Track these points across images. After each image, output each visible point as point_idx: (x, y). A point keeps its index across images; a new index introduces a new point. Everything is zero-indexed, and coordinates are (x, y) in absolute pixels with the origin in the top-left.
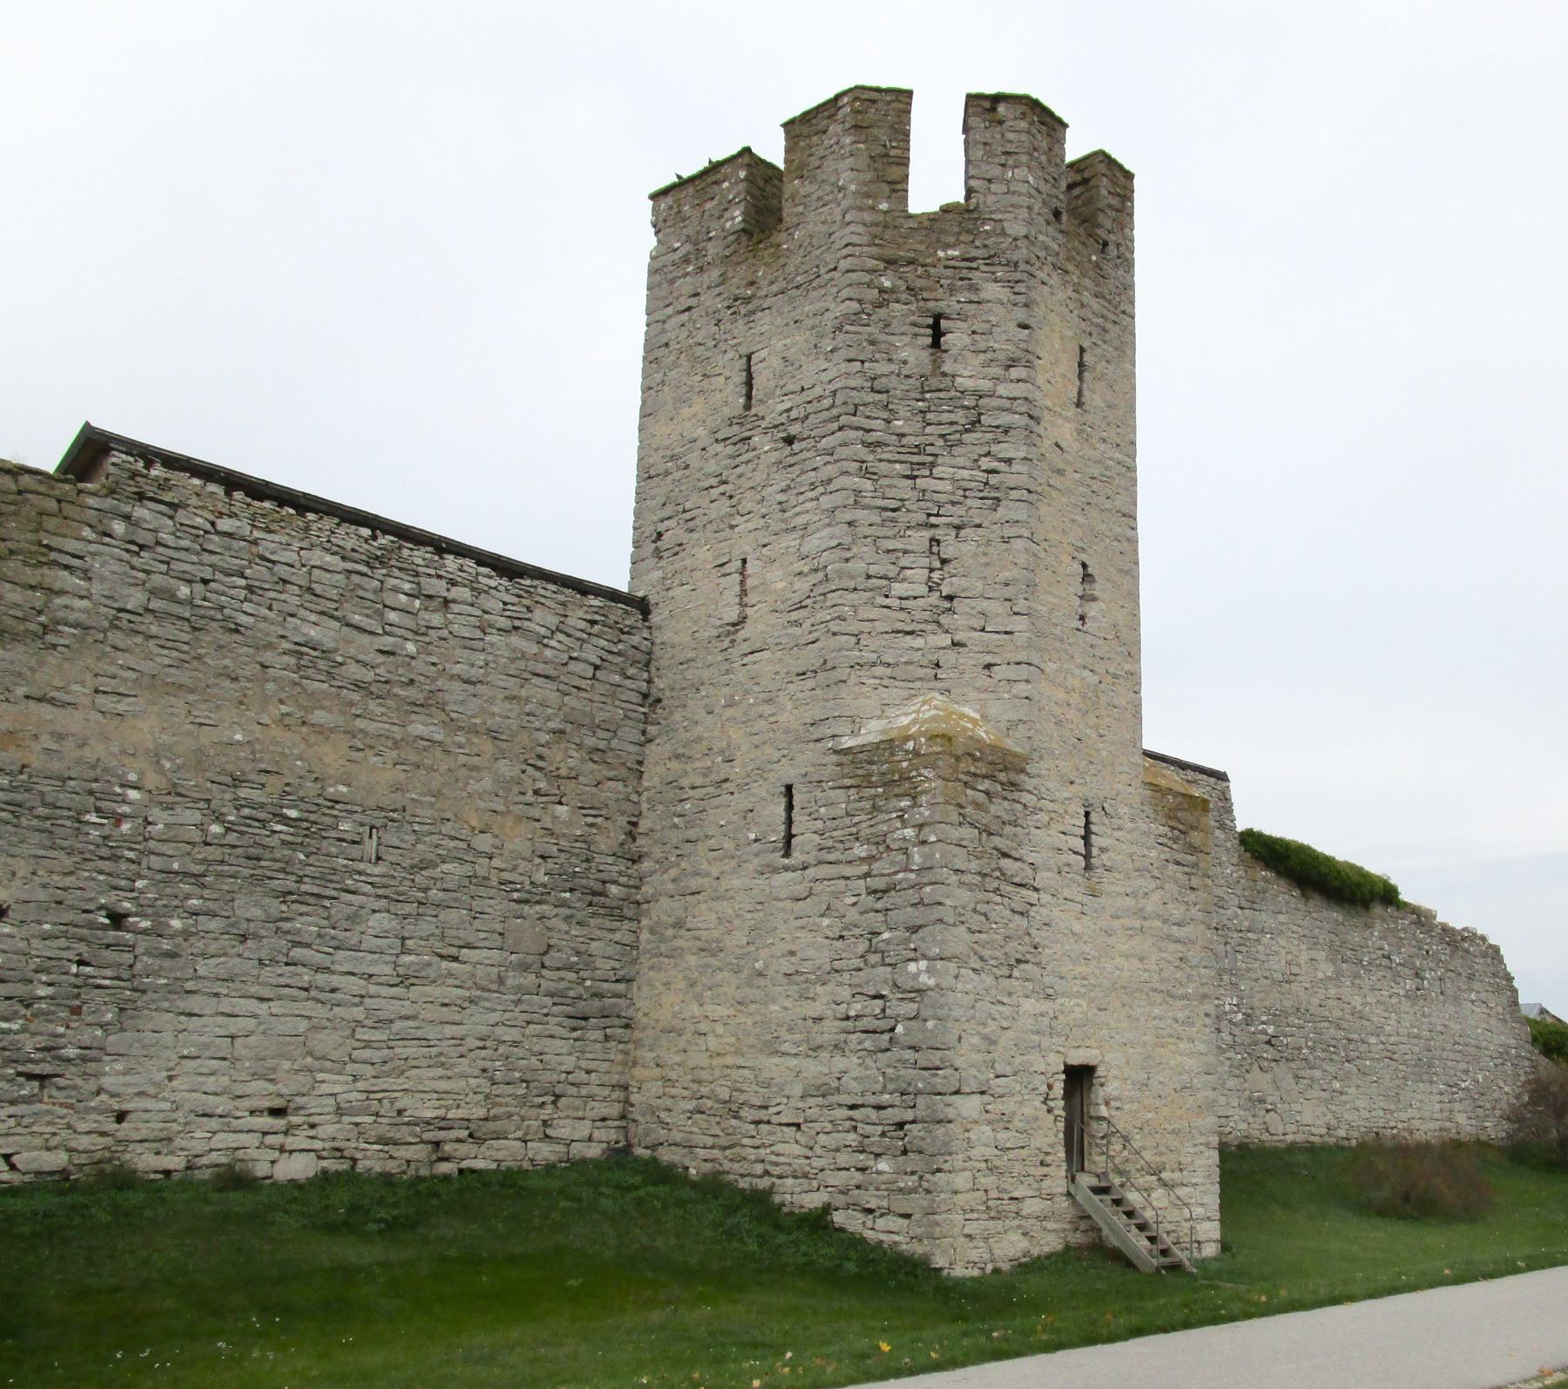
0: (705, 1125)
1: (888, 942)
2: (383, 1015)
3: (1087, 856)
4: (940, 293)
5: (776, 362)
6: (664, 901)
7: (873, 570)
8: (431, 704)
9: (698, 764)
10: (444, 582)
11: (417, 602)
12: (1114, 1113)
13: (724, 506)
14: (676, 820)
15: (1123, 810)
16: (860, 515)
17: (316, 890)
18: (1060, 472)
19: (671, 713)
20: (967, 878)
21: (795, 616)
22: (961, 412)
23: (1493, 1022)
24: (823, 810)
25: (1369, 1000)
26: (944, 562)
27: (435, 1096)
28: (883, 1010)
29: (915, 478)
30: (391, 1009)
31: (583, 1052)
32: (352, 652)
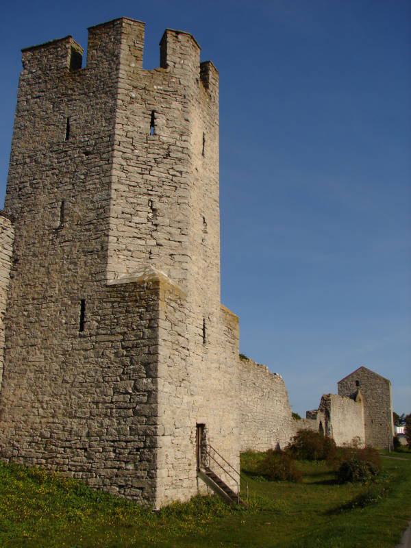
3: (204, 337)
7: (126, 210)
15: (215, 319)
18: (197, 180)
20: (168, 343)
22: (162, 150)
29: (143, 174)
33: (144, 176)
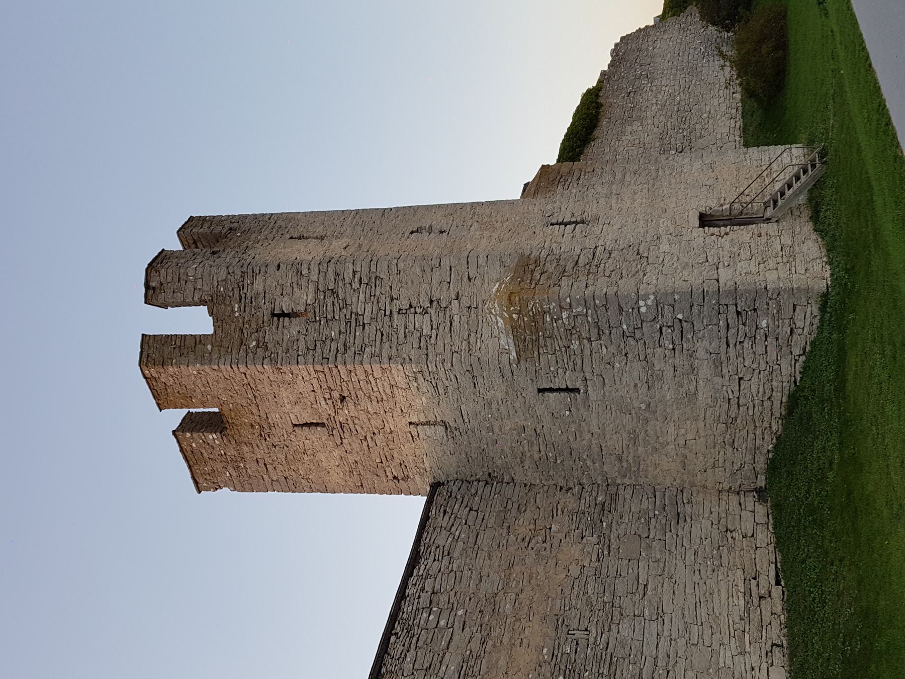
0: (741, 440)
1: (628, 326)
2: (682, 628)
3: (577, 223)
4: (260, 314)
5: (297, 409)
6: (606, 468)
7: (416, 345)
8: (493, 601)
9: (526, 449)
10: (423, 595)
11: (435, 609)
12: (727, 202)
13: (379, 438)
14: (559, 462)
16: (385, 354)
17: (607, 666)
18: (360, 246)
19: (497, 467)
20: (591, 282)
21: (441, 391)
23: (665, 37)
24: (552, 369)
25: (654, 102)
26: (411, 306)
27: (731, 598)
28: (669, 327)
30: (678, 623)
31: (699, 515)
32: (464, 645)
33: (366, 322)
